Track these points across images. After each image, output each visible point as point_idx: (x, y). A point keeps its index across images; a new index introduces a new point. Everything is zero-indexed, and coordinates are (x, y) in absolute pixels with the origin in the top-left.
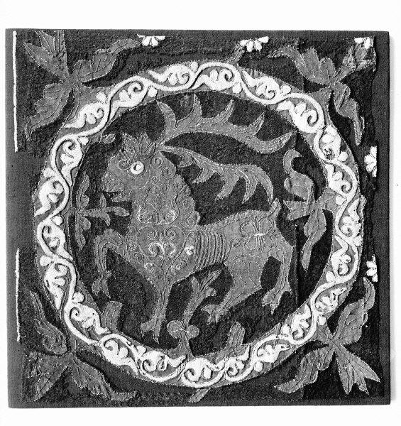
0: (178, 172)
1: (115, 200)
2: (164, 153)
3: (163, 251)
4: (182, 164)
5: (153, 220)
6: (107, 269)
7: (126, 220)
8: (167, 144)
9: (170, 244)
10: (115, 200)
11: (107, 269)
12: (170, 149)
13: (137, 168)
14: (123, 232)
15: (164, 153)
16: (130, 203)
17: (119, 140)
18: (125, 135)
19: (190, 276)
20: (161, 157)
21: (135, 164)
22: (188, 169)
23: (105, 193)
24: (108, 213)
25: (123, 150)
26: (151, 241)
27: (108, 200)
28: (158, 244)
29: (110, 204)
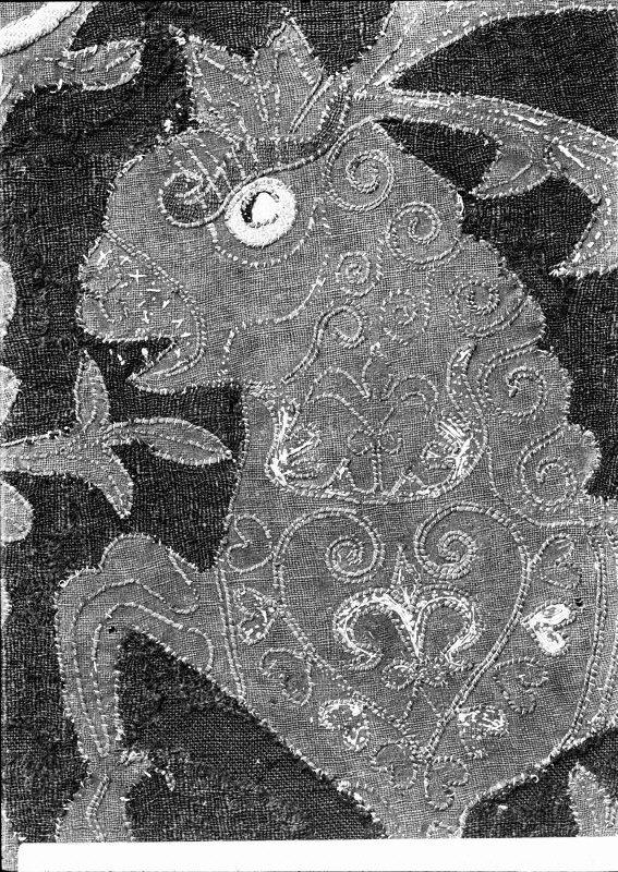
0: (472, 227)
1: (153, 380)
2: (397, 128)
3: (416, 641)
4: (502, 181)
5: (362, 478)
6: (128, 742)
7: (213, 488)
8: (407, 82)
9: (451, 599)
10: (153, 380)
11: (128, 742)
12: (427, 105)
13: (258, 213)
14: (201, 549)
15: (397, 128)
16: (232, 396)
17: (163, 69)
18: (192, 44)
19: (557, 761)
20: (386, 159)
21: (247, 191)
22: (523, 210)
23: (99, 349)
24: (120, 451)
25: (182, 123)
26: (353, 589)
27: (117, 382)
28: (386, 602)
29: (126, 402)
